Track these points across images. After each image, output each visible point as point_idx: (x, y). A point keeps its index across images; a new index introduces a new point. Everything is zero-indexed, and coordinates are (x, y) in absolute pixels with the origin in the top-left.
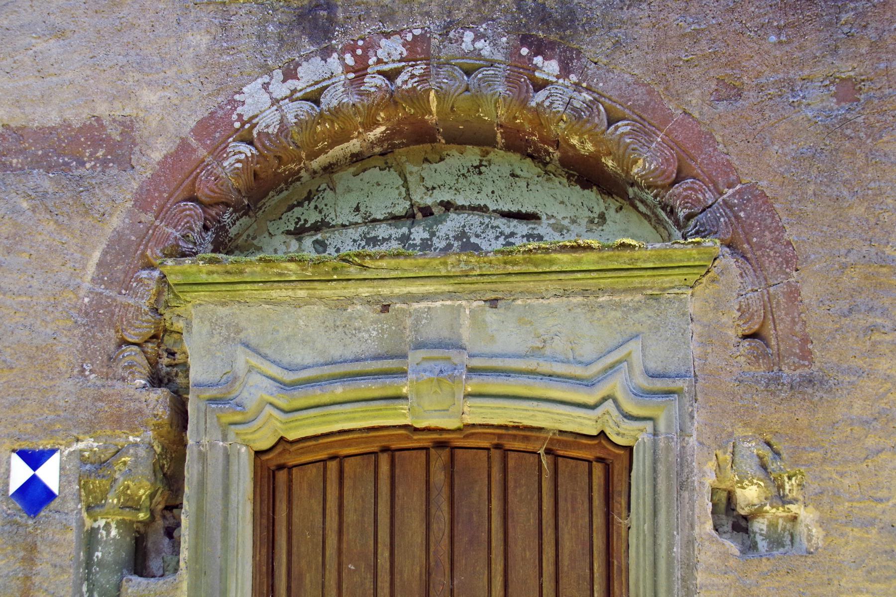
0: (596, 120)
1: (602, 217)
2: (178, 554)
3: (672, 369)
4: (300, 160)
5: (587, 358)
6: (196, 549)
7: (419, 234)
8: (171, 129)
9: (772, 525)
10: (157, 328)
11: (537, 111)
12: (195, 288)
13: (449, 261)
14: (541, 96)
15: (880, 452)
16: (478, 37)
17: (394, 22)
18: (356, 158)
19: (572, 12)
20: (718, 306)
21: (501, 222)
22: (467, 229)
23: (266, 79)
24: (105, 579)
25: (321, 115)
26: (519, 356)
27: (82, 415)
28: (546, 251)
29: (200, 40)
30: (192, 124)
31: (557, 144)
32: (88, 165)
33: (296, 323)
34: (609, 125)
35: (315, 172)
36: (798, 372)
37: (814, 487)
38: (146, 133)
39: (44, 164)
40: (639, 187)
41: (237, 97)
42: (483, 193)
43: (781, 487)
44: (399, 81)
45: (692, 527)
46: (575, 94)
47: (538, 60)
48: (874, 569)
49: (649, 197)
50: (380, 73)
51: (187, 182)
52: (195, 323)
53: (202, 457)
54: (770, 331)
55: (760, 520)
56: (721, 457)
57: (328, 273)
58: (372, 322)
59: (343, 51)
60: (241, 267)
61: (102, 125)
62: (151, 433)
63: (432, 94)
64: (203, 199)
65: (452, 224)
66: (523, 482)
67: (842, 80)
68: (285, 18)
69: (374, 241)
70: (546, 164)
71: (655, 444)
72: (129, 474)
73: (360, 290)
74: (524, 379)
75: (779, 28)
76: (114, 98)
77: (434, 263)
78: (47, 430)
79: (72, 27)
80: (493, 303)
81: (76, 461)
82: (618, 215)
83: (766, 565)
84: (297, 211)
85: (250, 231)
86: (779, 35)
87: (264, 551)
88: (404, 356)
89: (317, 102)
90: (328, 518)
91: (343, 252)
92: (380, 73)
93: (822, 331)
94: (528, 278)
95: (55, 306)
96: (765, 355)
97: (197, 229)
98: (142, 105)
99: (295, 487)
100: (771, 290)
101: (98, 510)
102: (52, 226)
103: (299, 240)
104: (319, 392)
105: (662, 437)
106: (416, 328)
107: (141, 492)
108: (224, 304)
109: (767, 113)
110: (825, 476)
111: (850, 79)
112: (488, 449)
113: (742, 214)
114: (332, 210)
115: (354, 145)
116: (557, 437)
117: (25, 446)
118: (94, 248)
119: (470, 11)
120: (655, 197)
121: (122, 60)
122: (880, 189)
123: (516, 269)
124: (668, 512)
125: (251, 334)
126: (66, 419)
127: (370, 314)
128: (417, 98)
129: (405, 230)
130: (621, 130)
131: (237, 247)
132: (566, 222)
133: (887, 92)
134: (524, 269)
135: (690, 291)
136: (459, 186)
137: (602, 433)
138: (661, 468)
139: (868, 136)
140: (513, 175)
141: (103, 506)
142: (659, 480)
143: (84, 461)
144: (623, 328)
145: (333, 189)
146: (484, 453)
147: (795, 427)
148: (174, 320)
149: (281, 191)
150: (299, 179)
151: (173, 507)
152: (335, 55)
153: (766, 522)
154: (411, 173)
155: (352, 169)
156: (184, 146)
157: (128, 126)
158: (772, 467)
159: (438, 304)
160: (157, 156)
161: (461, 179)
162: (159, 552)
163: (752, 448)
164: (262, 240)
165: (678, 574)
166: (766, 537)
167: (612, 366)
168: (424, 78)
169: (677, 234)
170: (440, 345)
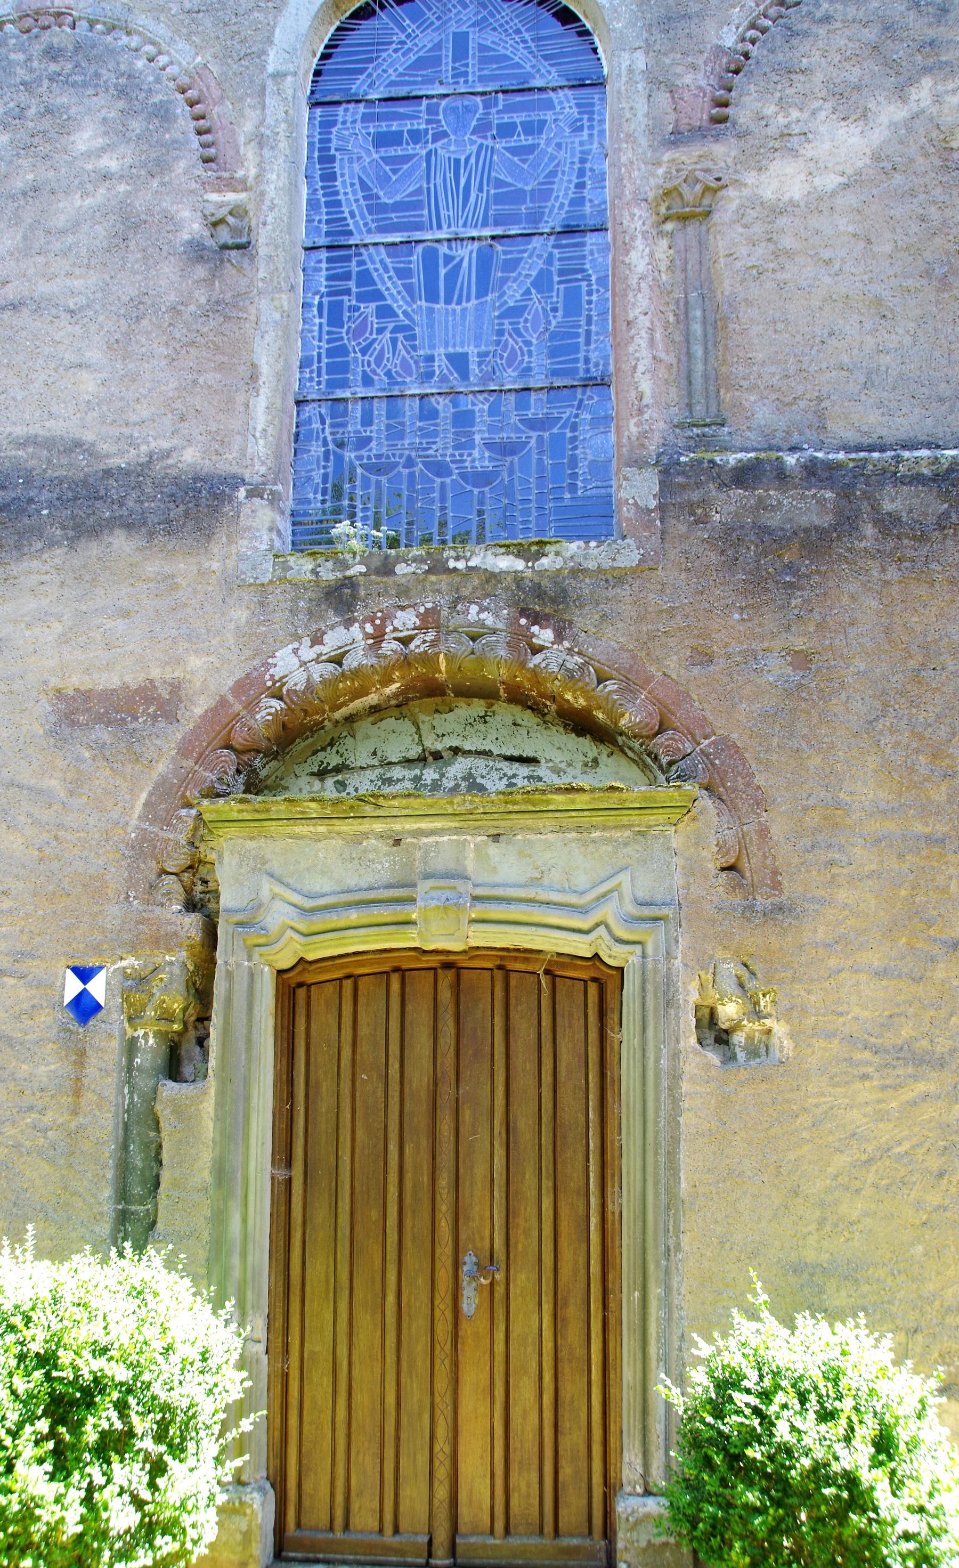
0: (587, 679)
1: (595, 761)
2: (207, 1062)
3: (658, 898)
4: (324, 712)
5: (581, 888)
6: (223, 1059)
7: (430, 775)
8: (212, 688)
9: (750, 1038)
10: (193, 860)
11: (535, 671)
12: (227, 824)
13: (455, 801)
14: (538, 659)
15: (840, 971)
16: (482, 610)
17: (409, 598)
18: (375, 710)
19: (564, 591)
20: (699, 842)
21: (504, 765)
22: (473, 771)
23: (296, 645)
24: (144, 1083)
25: (343, 674)
26: (520, 886)
27: (126, 936)
28: (543, 792)
29: (241, 615)
30: (230, 683)
31: (553, 699)
32: (141, 720)
33: (316, 856)
34: (599, 683)
35: (337, 722)
36: (769, 901)
37: (785, 1003)
38: (191, 692)
39: (104, 720)
40: (627, 736)
41: (270, 661)
42: (488, 740)
43: (756, 1003)
44: (412, 646)
45: (678, 1041)
46: (568, 657)
47: (535, 629)
48: (836, 1075)
49: (636, 745)
50: (395, 639)
51: (224, 732)
52: (226, 855)
53: (230, 975)
54: (745, 865)
55: (739, 1033)
56: (703, 977)
57: (345, 811)
58: (385, 855)
59: (364, 621)
60: (268, 806)
61: (154, 686)
62: (184, 953)
63: (442, 656)
64: (237, 746)
65: (459, 767)
66: (524, 1000)
67: (796, 652)
68: (314, 596)
69: (389, 781)
70: (544, 715)
71: (643, 965)
72: (165, 990)
73: (375, 826)
74: (523, 907)
75: (741, 608)
76: (167, 663)
77: (441, 802)
78: (97, 949)
79: (136, 608)
80: (496, 837)
81: (120, 978)
82: (610, 760)
83: (743, 1074)
84: (321, 755)
85: (279, 774)
86: (741, 614)
87: (284, 1061)
88: (414, 885)
89: (340, 664)
90: (343, 1032)
91: (361, 792)
92: (395, 639)
93: (790, 864)
94: (527, 816)
95: (107, 841)
96: (741, 886)
97: (231, 773)
98: (189, 669)
99: (313, 1003)
100: (745, 827)
101: (137, 1021)
102: (108, 772)
103: (322, 780)
104: (335, 918)
105: (650, 959)
106: (425, 858)
107: (176, 1005)
108: (252, 838)
109: (735, 677)
110: (795, 993)
111: (802, 651)
112: (491, 970)
113: (717, 762)
114: (351, 755)
115: (372, 699)
116: (555, 958)
117: (78, 963)
118: (142, 790)
119: (475, 588)
120: (641, 745)
121: (174, 632)
122: (832, 743)
123: (516, 808)
124: (655, 1028)
125: (275, 865)
126: (112, 940)
127: (383, 847)
128: (428, 659)
129: (417, 772)
130: (609, 688)
131: (266, 787)
132: (563, 766)
133: (833, 663)
134: (523, 808)
135: (673, 828)
136: (466, 733)
137: (596, 956)
138: (650, 987)
139: (820, 699)
140: (515, 724)
141: (142, 1017)
142: (648, 999)
143: (127, 977)
144: (614, 860)
145: (353, 736)
146: (488, 973)
147: (768, 950)
148: (208, 853)
149: (307, 738)
150: (323, 728)
151: (204, 1019)
152: (357, 625)
153: (744, 1035)
154: (423, 722)
155: (371, 719)
156: (223, 702)
157: (176, 687)
158: (748, 985)
159: (446, 838)
160: (199, 711)
161: (468, 728)
162: (191, 1059)
163: (730, 969)
164: (289, 781)
165: (665, 1084)
166: (745, 1049)
167: (604, 895)
168: (434, 644)
169: (662, 777)
170: (448, 876)
